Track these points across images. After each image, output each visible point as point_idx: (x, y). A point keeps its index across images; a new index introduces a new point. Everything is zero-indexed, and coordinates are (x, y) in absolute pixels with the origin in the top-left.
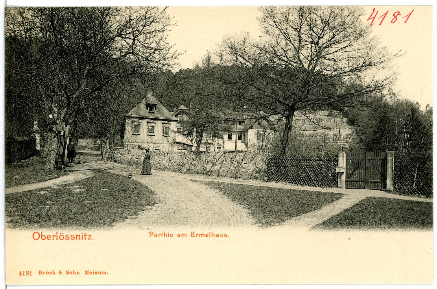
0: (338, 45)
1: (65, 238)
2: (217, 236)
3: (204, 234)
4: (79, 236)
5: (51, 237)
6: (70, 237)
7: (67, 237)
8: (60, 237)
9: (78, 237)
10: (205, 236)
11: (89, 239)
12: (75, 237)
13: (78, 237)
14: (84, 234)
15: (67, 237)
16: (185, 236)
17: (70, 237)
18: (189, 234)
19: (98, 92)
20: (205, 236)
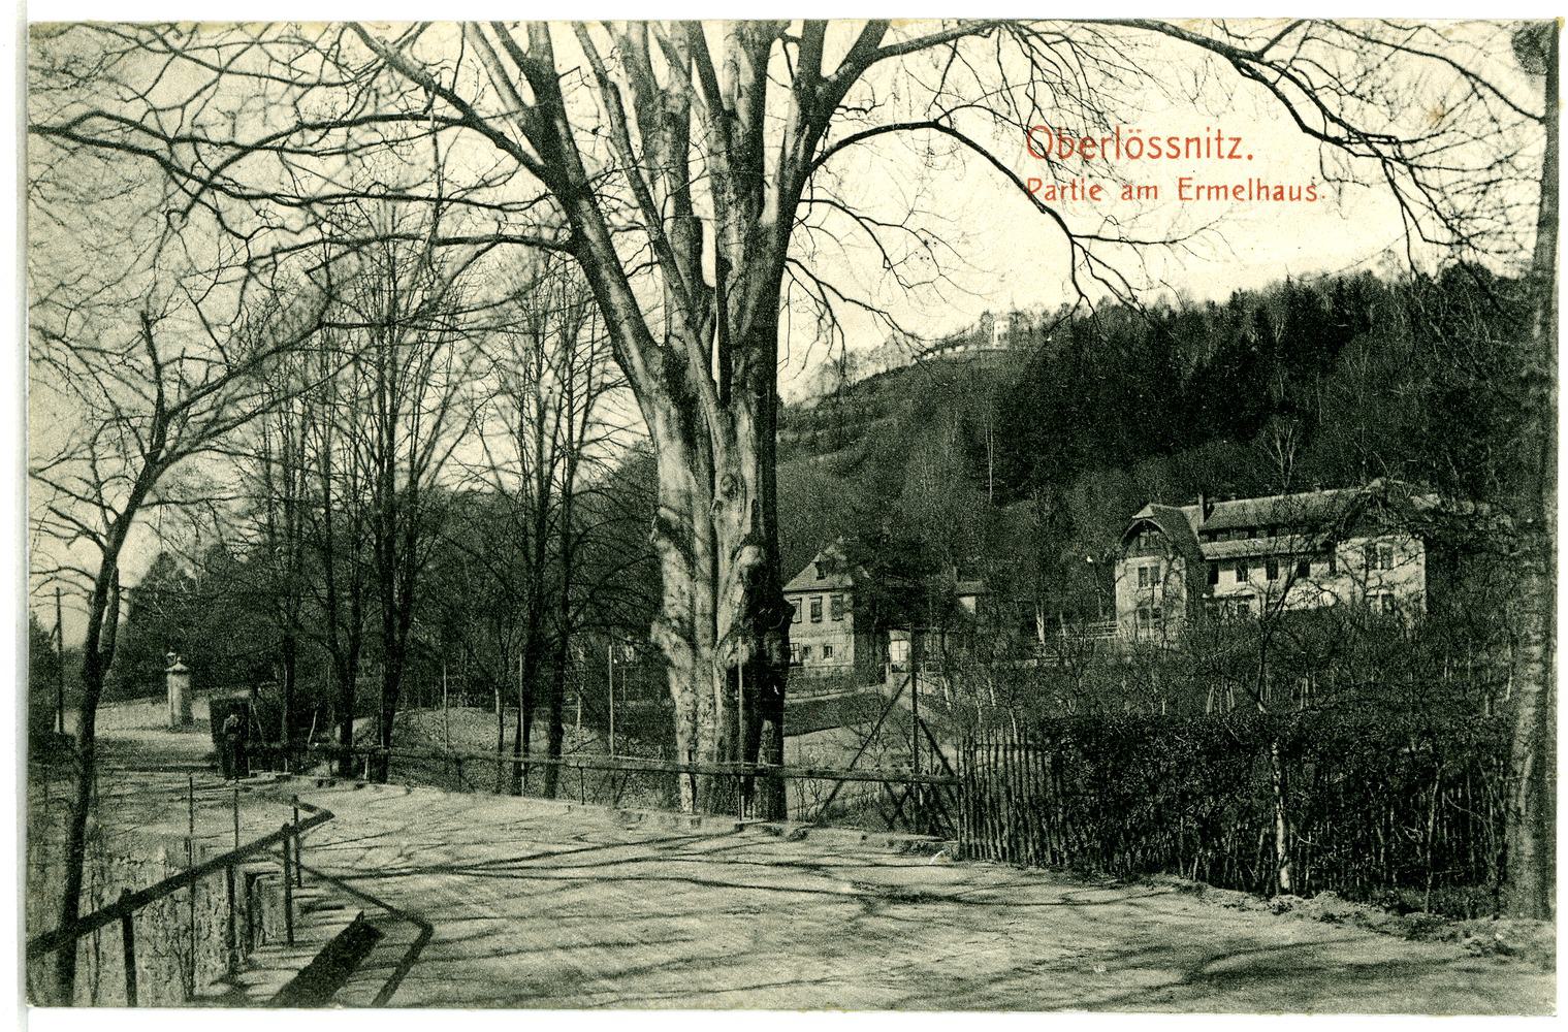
0: (722, 444)
1: (1148, 149)
2: (1279, 195)
3: (1225, 187)
4: (1194, 144)
5: (1094, 144)
6: (1165, 148)
7: (1174, 147)
8: (296, 229)
9: (1193, 146)
10: (1230, 193)
11: (1231, 156)
12: (1181, 145)
13: (1193, 146)
14: (1213, 135)
15: (1174, 147)
16: (1152, 191)
17: (1165, 148)
18: (1169, 190)
19: (364, 656)
20: (1230, 193)
